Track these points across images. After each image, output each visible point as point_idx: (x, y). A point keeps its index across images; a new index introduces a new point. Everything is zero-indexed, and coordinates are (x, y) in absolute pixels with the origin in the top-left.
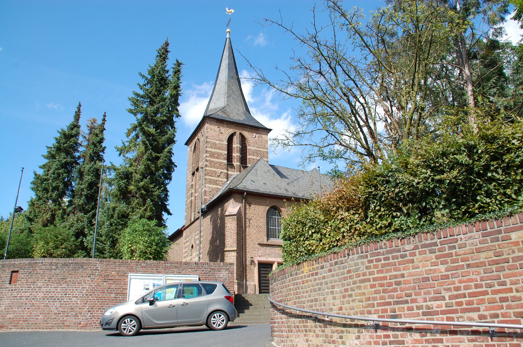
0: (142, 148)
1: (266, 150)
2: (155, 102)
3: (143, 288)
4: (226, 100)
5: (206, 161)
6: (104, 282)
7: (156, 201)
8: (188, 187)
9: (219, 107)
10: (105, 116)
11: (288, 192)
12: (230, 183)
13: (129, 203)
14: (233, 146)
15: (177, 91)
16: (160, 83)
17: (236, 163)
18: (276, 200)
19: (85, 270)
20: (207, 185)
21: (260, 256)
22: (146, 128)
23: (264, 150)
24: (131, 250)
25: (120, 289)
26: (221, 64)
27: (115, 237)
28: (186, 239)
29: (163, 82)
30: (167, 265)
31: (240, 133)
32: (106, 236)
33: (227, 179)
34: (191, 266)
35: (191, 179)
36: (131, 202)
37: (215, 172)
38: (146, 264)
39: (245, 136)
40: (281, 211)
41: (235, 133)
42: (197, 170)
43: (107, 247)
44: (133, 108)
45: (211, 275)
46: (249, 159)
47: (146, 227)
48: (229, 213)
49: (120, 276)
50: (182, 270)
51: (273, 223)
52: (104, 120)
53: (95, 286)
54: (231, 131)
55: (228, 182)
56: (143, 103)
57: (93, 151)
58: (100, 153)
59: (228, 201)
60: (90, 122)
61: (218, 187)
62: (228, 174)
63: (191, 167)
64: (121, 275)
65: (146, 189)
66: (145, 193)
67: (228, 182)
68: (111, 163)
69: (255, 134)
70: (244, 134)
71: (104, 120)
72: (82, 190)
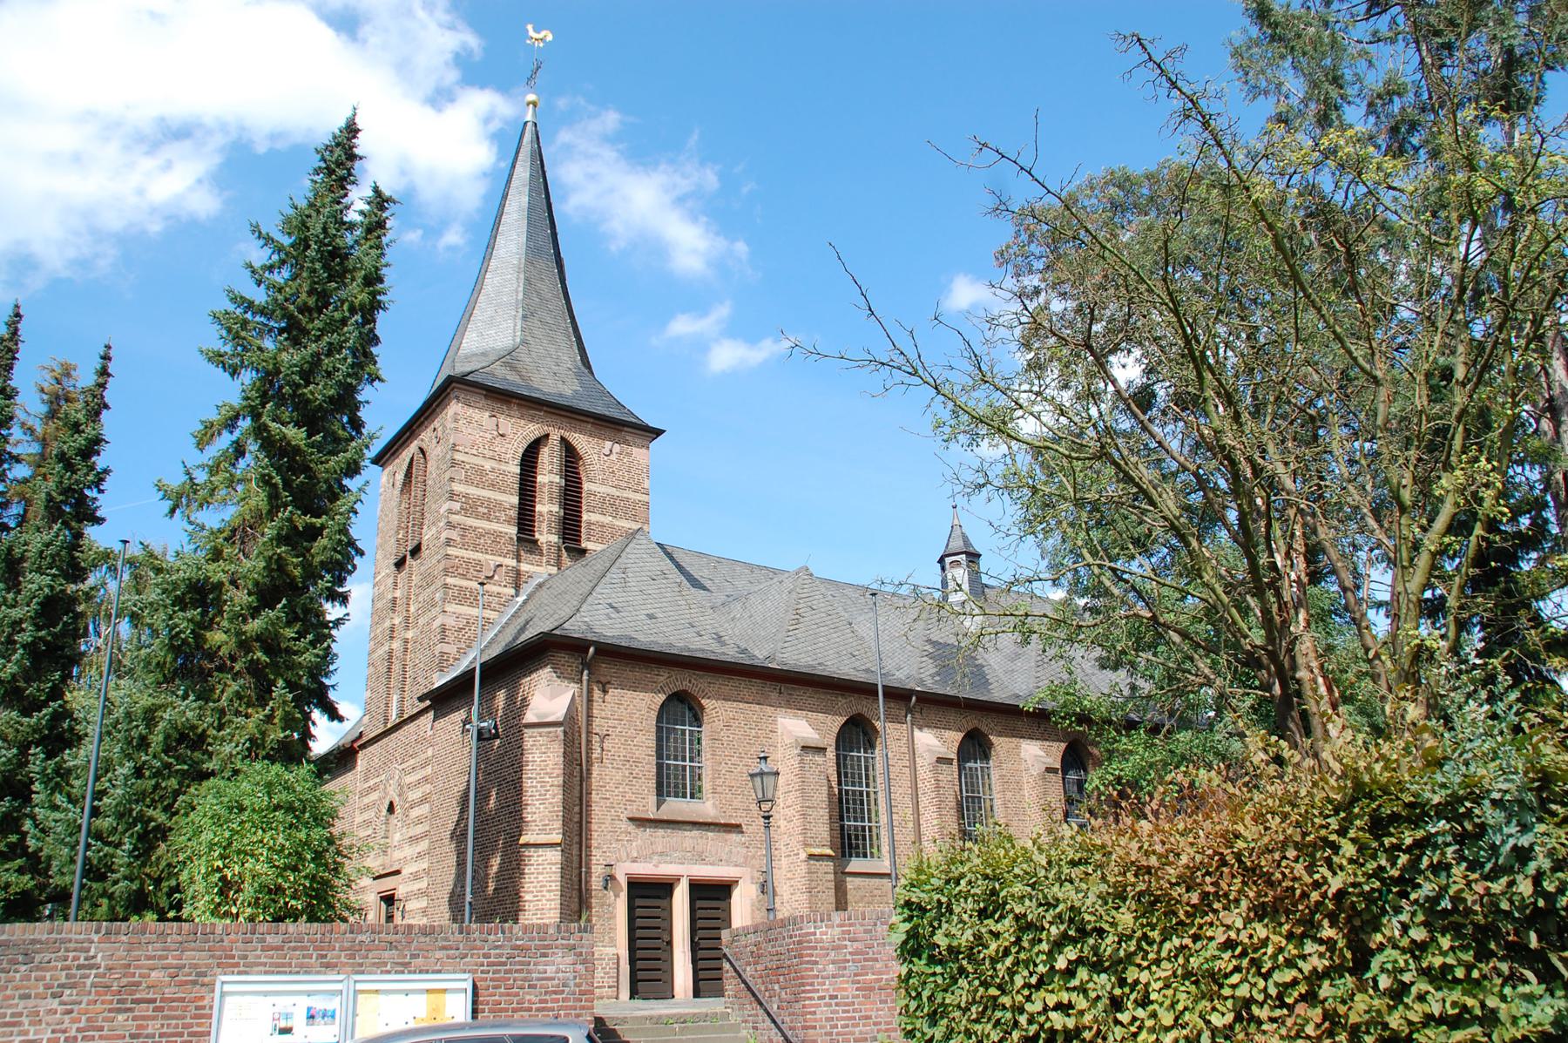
0: (259, 499)
1: (644, 498)
2: (306, 332)
3: (270, 1029)
4: (519, 327)
5: (450, 526)
6: (119, 1011)
7: (302, 687)
8: (379, 605)
9: (494, 349)
10: (107, 358)
11: (724, 644)
12: (525, 602)
13: (205, 696)
14: (539, 478)
15: (374, 294)
16: (326, 267)
17: (547, 536)
18: (687, 673)
19: (38, 968)
20: (450, 608)
21: (634, 860)
22: (274, 425)
23: (638, 497)
24: (223, 879)
25: (181, 1035)
26: (502, 206)
27: (151, 819)
28: (366, 780)
29: (335, 261)
30: (360, 937)
31: (563, 439)
32: (120, 816)
33: (517, 587)
34: (446, 939)
35: (390, 581)
36: (213, 690)
37: (479, 563)
38: (280, 937)
39: (579, 447)
40: (702, 708)
41: (547, 436)
42: (416, 551)
43: (121, 857)
44: (228, 349)
45: (516, 971)
46: (589, 523)
47: (281, 797)
48: (538, 716)
49: (182, 984)
50: (414, 956)
51: (676, 748)
52: (104, 372)
53: (78, 1030)
54: (533, 430)
55: (520, 599)
56: (261, 334)
57: (61, 483)
58: (87, 492)
59: (531, 672)
60: (48, 376)
61: (488, 614)
62: (518, 573)
63: (393, 540)
64: (186, 983)
65: (269, 642)
66: (265, 658)
67: (520, 599)
68: (145, 547)
69: (608, 444)
70: (574, 443)
71: (104, 372)
72: (16, 625)
